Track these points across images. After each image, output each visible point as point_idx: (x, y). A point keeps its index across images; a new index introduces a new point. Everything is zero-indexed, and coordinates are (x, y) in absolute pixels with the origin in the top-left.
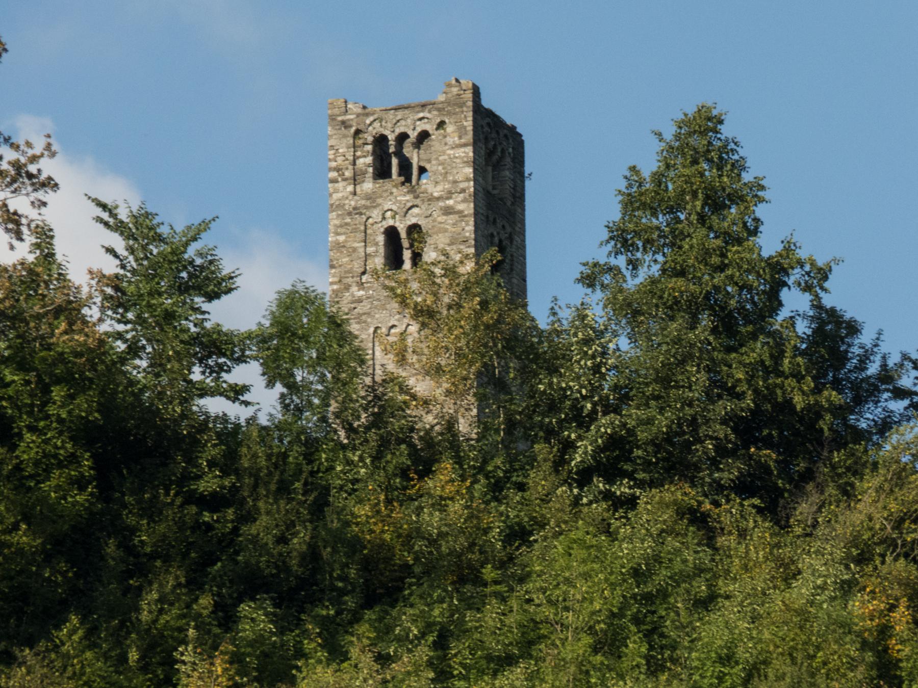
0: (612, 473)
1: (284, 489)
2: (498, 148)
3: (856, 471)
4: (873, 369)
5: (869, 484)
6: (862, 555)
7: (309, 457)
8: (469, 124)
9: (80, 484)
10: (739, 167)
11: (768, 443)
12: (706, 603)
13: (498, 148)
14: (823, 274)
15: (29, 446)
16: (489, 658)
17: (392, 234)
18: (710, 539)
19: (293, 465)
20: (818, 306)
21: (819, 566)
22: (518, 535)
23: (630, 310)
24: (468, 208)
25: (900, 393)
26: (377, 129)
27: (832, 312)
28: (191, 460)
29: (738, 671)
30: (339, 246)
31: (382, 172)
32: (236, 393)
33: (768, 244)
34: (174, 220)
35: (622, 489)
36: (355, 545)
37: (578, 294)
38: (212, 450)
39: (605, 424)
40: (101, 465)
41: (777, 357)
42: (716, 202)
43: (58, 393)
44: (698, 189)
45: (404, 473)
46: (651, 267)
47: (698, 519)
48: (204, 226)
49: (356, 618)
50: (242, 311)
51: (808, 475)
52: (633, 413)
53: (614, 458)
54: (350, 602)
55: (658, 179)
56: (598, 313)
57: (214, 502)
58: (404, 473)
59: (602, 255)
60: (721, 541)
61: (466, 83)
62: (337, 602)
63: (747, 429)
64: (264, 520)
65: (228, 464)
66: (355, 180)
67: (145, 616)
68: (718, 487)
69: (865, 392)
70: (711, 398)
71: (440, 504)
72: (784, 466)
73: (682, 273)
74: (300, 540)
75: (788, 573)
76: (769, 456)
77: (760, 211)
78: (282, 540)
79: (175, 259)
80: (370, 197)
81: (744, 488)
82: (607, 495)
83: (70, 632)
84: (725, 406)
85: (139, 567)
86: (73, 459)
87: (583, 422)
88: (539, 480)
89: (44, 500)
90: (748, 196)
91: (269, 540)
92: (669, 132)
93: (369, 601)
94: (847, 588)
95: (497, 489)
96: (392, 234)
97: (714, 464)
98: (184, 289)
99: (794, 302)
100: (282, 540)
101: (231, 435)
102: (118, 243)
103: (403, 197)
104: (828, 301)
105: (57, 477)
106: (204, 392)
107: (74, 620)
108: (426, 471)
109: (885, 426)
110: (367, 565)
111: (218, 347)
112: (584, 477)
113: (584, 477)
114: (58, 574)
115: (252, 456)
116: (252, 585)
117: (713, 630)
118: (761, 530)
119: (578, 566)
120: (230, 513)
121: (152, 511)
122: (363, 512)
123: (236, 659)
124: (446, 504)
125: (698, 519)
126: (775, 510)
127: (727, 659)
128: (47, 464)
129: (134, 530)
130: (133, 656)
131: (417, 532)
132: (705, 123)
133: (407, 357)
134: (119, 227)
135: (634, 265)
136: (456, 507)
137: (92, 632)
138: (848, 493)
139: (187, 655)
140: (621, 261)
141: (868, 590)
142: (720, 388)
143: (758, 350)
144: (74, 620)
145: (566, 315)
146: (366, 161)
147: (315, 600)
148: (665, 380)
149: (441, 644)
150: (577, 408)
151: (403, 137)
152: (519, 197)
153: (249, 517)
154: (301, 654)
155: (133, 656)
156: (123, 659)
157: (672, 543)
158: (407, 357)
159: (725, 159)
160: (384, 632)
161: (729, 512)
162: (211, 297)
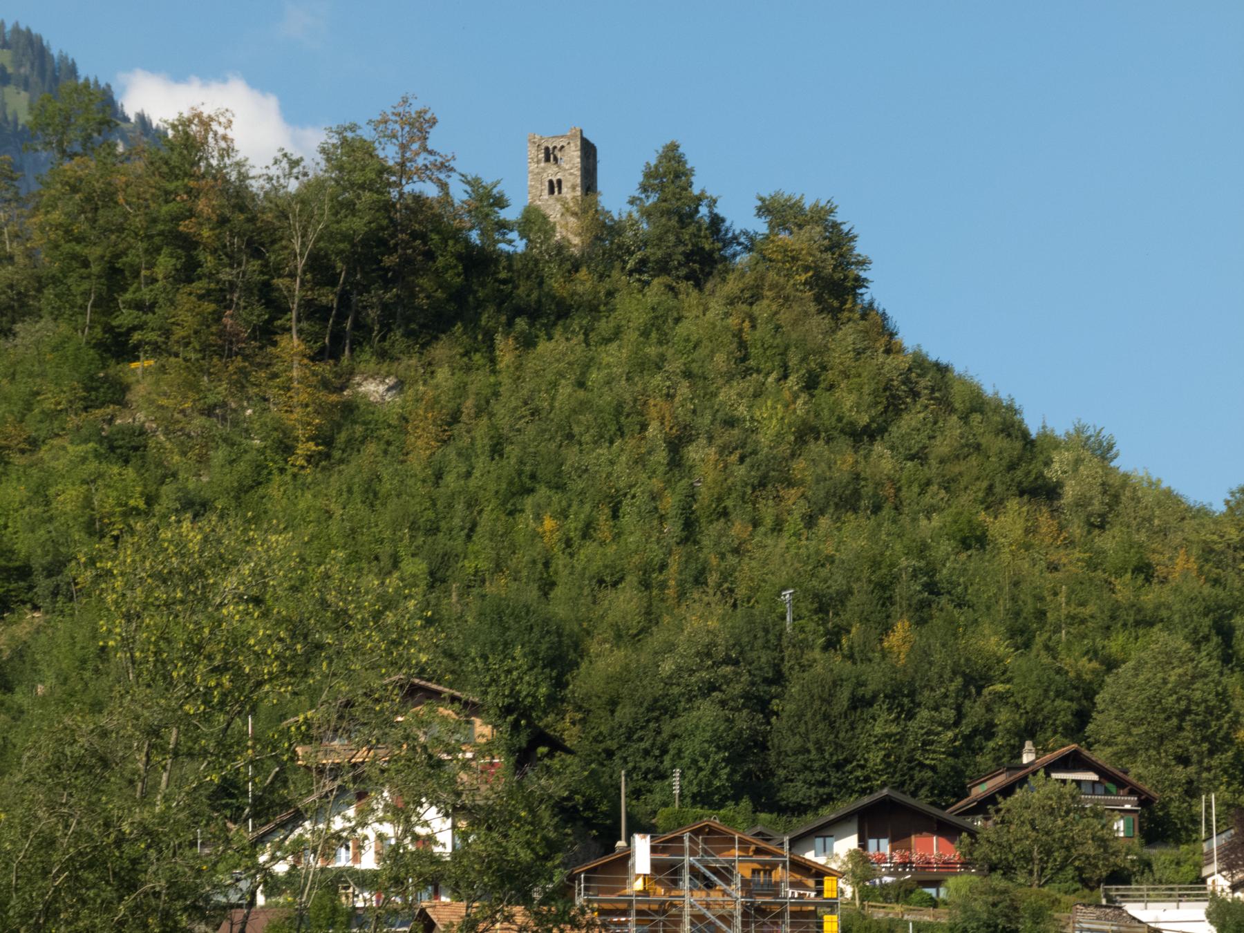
0: (640, 272)
1: (528, 277)
2: (588, 151)
3: (727, 271)
4: (730, 235)
5: (731, 277)
6: (731, 302)
7: (536, 265)
8: (579, 143)
9: (458, 275)
10: (685, 162)
11: (695, 262)
12: (678, 320)
13: (588, 151)
14: (715, 202)
15: (440, 262)
16: (603, 339)
17: (551, 182)
18: (676, 295)
19: (530, 268)
20: (711, 212)
21: (716, 307)
22: (610, 294)
23: (647, 214)
24: (578, 173)
25: (739, 244)
26: (545, 144)
27: (716, 215)
28: (496, 266)
29: (691, 345)
30: (532, 186)
31: (547, 160)
32: (510, 242)
33: (696, 191)
34: (487, 180)
35: (645, 277)
36: (553, 298)
37: (628, 208)
38: (504, 263)
39: (639, 255)
40: (466, 268)
41: (699, 230)
42: (677, 176)
43: (451, 242)
44: (670, 173)
45: (569, 271)
46: (653, 198)
47: (671, 289)
48: (498, 182)
49: (555, 324)
50: (510, 214)
51: (710, 273)
52: (649, 250)
53: (642, 266)
54: (552, 318)
55: (656, 167)
56: (636, 215)
57: (505, 282)
58: (569, 271)
59: (637, 194)
60: (680, 296)
61: (578, 128)
62: (548, 318)
63: (688, 256)
64: (522, 288)
65: (509, 268)
66: (538, 162)
67: (483, 323)
68: (678, 277)
69: (727, 243)
70: (675, 246)
71: (583, 283)
72: (702, 270)
73: (665, 201)
74: (534, 296)
75: (706, 310)
76: (697, 266)
77: (693, 179)
78: (528, 295)
79: (489, 195)
80: (544, 169)
81: (687, 278)
82: (639, 280)
83: (458, 328)
84: (681, 249)
85: (480, 305)
86: (456, 266)
87: (632, 254)
88: (615, 274)
89: (446, 281)
90: (688, 173)
91: (524, 296)
92: (660, 151)
93: (559, 317)
94: (727, 315)
95: (601, 277)
96: (551, 182)
97: (677, 269)
98: (492, 205)
99: (703, 210)
100: (528, 295)
101: (509, 257)
102: (469, 189)
103: (555, 169)
104: (716, 211)
105: (450, 273)
106: (500, 242)
107: (459, 324)
108: (577, 271)
109: (734, 255)
110: (558, 304)
111: (503, 226)
112: (631, 273)
113: (631, 273)
114: (452, 307)
115: (517, 265)
116: (518, 312)
117: (681, 330)
118: (695, 293)
119: (635, 304)
120: (510, 286)
121: (483, 285)
122: (556, 284)
123: (516, 339)
124: (584, 282)
125: (671, 289)
126: (699, 285)
127: (687, 340)
128: (447, 268)
129: (477, 291)
130: (480, 337)
131: (574, 293)
132: (673, 147)
133: (569, 232)
134: (468, 183)
135: (648, 197)
136: (588, 284)
137: (465, 328)
138: (724, 280)
139: (498, 337)
140: (643, 196)
141: (95, 135)
142: (679, 242)
143: (692, 229)
144: (459, 324)
145: (624, 215)
146: (542, 156)
147: (540, 317)
148: (660, 239)
149: (586, 335)
150: (628, 249)
151: (555, 148)
152: (595, 169)
153: (516, 287)
154: (537, 337)
155: (480, 337)
156: (476, 338)
157: (664, 298)
158: (569, 232)
159: (680, 160)
160: (566, 329)
161: (683, 286)
162: (502, 208)
